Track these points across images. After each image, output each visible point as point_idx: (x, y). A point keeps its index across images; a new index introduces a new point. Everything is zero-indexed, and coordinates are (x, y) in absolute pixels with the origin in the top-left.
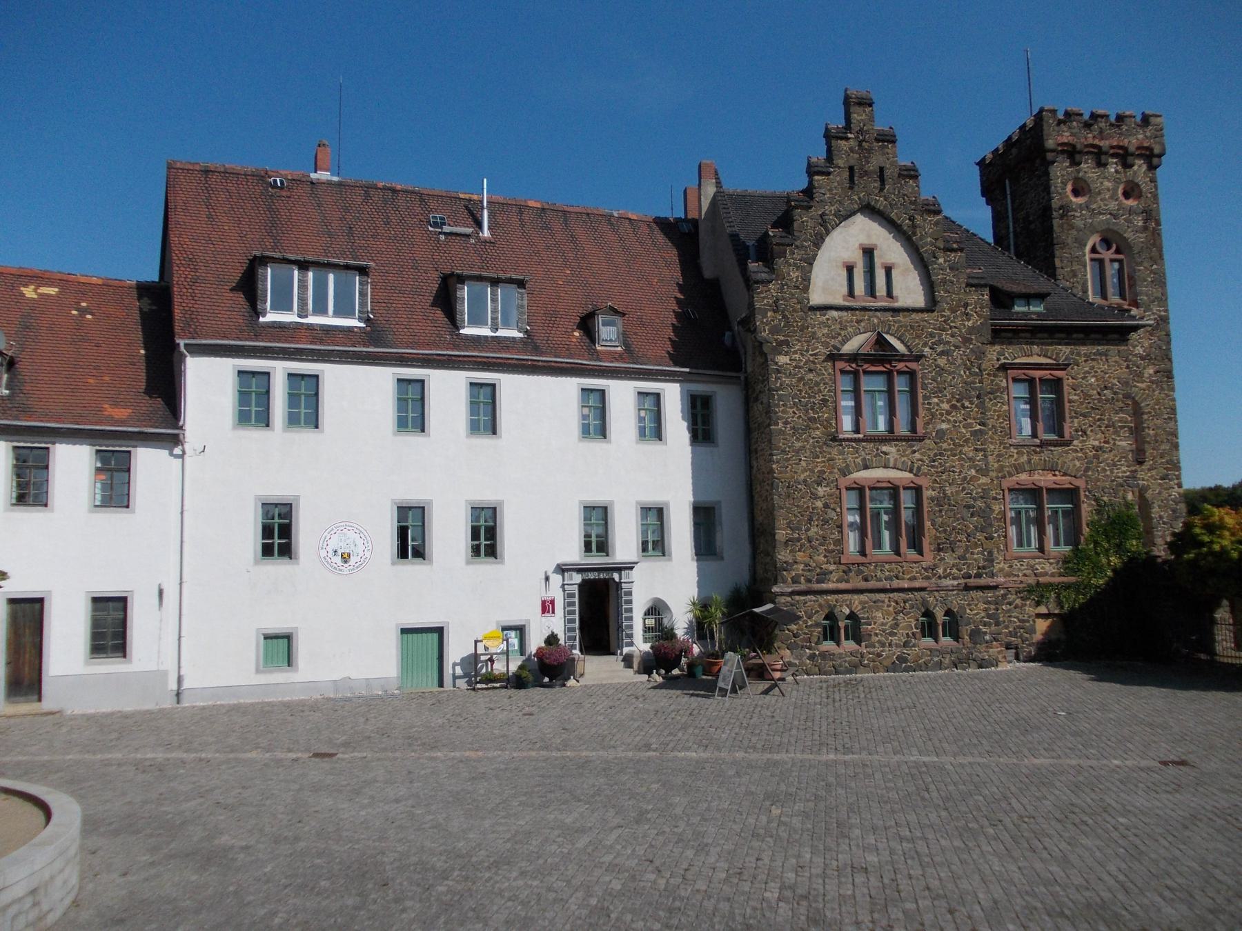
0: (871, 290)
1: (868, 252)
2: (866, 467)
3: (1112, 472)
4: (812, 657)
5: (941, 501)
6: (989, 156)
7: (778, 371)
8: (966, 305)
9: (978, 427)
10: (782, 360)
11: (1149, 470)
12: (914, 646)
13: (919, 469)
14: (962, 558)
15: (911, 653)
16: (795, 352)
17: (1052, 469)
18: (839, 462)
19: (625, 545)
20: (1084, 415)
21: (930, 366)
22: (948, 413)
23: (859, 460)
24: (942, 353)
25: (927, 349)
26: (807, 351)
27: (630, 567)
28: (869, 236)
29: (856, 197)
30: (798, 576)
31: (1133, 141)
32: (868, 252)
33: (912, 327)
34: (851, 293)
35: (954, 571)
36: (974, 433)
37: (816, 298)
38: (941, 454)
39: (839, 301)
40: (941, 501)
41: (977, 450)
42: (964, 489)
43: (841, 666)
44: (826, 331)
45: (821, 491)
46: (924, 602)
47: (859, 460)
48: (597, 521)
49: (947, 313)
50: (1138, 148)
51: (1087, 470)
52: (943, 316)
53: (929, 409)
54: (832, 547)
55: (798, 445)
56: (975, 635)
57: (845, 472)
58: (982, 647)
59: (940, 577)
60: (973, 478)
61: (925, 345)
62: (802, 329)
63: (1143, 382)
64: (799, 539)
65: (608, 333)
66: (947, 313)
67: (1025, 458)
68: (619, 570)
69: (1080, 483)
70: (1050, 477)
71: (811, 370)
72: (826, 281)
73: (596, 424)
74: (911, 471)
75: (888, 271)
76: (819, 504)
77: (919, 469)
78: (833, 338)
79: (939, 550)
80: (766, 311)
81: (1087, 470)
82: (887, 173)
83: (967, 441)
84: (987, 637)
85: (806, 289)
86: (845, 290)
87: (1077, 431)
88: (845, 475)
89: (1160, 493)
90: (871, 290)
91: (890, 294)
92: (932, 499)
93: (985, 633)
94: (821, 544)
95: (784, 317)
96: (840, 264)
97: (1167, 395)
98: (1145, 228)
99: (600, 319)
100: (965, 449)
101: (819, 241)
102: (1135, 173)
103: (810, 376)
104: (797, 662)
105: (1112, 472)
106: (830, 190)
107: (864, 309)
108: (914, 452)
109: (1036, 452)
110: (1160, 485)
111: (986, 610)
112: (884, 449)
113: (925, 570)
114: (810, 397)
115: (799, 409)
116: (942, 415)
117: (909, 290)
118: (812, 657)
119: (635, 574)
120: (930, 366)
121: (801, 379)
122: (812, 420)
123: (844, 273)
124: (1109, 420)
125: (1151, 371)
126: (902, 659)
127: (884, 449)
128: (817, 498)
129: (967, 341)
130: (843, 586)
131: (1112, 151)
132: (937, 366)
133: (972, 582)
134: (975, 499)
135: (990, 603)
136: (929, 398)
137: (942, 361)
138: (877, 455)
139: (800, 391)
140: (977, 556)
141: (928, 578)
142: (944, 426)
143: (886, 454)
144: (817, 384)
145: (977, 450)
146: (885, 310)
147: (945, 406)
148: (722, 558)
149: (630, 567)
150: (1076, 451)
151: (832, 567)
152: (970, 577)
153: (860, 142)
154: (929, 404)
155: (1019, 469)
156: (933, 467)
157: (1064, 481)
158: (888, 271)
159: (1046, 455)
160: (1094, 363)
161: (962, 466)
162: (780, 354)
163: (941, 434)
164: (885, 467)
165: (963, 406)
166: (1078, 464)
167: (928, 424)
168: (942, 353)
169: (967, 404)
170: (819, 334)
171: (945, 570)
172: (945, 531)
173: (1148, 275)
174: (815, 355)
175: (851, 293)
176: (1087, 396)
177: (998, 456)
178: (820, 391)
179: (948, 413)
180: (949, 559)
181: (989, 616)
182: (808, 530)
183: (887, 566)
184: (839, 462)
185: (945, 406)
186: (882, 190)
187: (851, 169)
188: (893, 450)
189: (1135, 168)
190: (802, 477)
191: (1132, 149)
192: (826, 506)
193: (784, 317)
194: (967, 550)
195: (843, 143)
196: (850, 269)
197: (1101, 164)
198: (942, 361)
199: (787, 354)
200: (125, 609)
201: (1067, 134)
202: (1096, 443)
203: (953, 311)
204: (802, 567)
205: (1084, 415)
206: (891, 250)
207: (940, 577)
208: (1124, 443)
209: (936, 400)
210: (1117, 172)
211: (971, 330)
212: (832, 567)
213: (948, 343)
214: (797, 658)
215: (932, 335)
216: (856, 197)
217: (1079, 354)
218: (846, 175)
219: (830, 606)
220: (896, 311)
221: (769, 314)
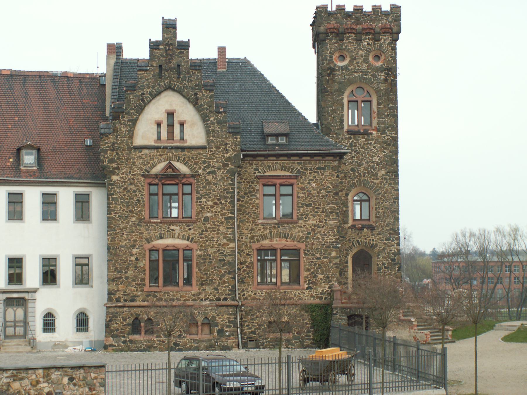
0: (170, 134)
1: (170, 115)
2: (161, 238)
3: (323, 239)
4: (124, 342)
5: (206, 257)
6: (349, 8)
7: (112, 185)
8: (226, 144)
9: (230, 215)
10: (115, 178)
11: (378, 234)
12: (184, 337)
13: (192, 239)
14: (216, 289)
15: (181, 341)
16: (123, 174)
17: (286, 237)
18: (146, 234)
19: (32, 276)
20: (307, 205)
21: (202, 180)
22: (212, 207)
23: (157, 234)
24: (209, 173)
25: (200, 171)
26: (130, 173)
27: (35, 291)
28: (171, 105)
29: (163, 84)
30: (119, 298)
31: (377, 26)
32: (170, 115)
33: (193, 158)
34: (159, 138)
35: (211, 296)
36: (226, 219)
37: (138, 141)
38: (206, 231)
39: (153, 144)
40: (206, 257)
41: (228, 228)
42: (219, 250)
43: (141, 347)
44: (141, 161)
45: (135, 251)
46: (192, 314)
47: (157, 234)
48: (15, 264)
49: (214, 149)
50: (382, 29)
51: (307, 238)
52: (211, 151)
53: (200, 205)
54: (139, 282)
55: (122, 226)
56: (221, 332)
57: (148, 241)
58: (223, 339)
59: (202, 300)
60: (225, 244)
61: (200, 168)
62: (127, 160)
63: (377, 179)
64: (121, 278)
65: (29, 159)
66: (214, 149)
67: (268, 231)
68: (27, 292)
69: (302, 246)
70: (284, 242)
71: (131, 184)
72: (145, 132)
73: (15, 209)
74: (188, 240)
75: (182, 125)
76: (133, 258)
77: (192, 239)
78: (145, 165)
79: (202, 284)
80: (107, 151)
81: (307, 238)
82: (183, 69)
83: (222, 223)
84: (227, 334)
85: (131, 137)
86: (155, 137)
87: (302, 215)
88: (149, 243)
89: (384, 249)
90: (170, 134)
91: (182, 139)
92: (200, 256)
93: (227, 331)
94: (134, 280)
95: (117, 154)
96: (153, 122)
97: (393, 188)
98: (386, 80)
99: (24, 152)
100: (221, 228)
101: (141, 109)
102: (381, 44)
103: (131, 187)
104: (116, 344)
105: (323, 239)
106: (147, 80)
107: (166, 148)
108: (190, 229)
109: (274, 227)
110: (385, 244)
111: (229, 318)
112: (172, 227)
113: (194, 295)
114: (130, 198)
115: (124, 206)
116: (208, 208)
117: (195, 135)
118: (124, 342)
119: (37, 295)
120: (202, 180)
121: (125, 189)
122: (131, 211)
123: (155, 127)
124: (323, 208)
125: (383, 172)
126: (176, 344)
127: (172, 227)
128: (132, 255)
129: (225, 165)
130: (145, 303)
131: (364, 32)
132: (207, 180)
133: (222, 302)
134: (226, 256)
135: (231, 314)
136: (201, 198)
137: (210, 178)
138: (168, 231)
139: (125, 195)
140: (224, 289)
141: (194, 300)
142: (209, 215)
143: (173, 230)
144: (135, 192)
145: (228, 228)
146: (177, 148)
147: (210, 203)
148: (92, 287)
149: (35, 291)
150: (301, 227)
151: (139, 293)
152: (220, 300)
153: (166, 51)
154: (200, 202)
155: (264, 237)
156: (201, 238)
157: (290, 244)
158: (182, 125)
159: (281, 230)
160: (315, 174)
161: (219, 237)
162: (114, 174)
163: (207, 219)
164: (173, 237)
165: (221, 203)
166: (301, 234)
167: (199, 213)
168: (209, 173)
169: (223, 202)
170: (137, 163)
171: (206, 296)
172: (207, 274)
173: (386, 111)
174: (134, 175)
175: (159, 138)
176: (310, 194)
177: (251, 230)
178: (136, 195)
179: (212, 207)
180: (209, 289)
181: (230, 322)
182: (126, 272)
183: (171, 293)
184: (146, 234)
185: (210, 203)
186: (179, 78)
187: (160, 66)
188: (178, 228)
189: (382, 41)
190: (124, 244)
191: (377, 30)
192: (137, 259)
193: (117, 154)
194: (219, 285)
195: (157, 51)
196: (159, 125)
197: (359, 40)
198: (210, 178)
199: (118, 174)
200: (21, 267)
201: (334, 22)
202: (314, 222)
203: (218, 148)
204: (122, 293)
205: (307, 205)
206: (186, 112)
207: (202, 300)
208: (332, 222)
209: (204, 200)
210: (368, 44)
211: (229, 159)
212: (139, 293)
213: (214, 166)
214: (116, 342)
215: (204, 162)
216: (163, 84)
217: (306, 169)
218: (157, 70)
219: (136, 314)
220: (183, 149)
221: (109, 152)
